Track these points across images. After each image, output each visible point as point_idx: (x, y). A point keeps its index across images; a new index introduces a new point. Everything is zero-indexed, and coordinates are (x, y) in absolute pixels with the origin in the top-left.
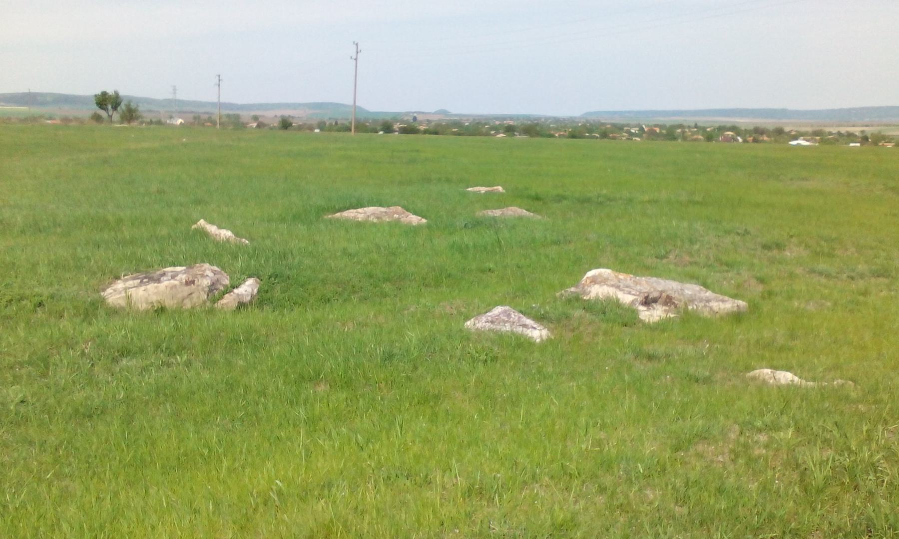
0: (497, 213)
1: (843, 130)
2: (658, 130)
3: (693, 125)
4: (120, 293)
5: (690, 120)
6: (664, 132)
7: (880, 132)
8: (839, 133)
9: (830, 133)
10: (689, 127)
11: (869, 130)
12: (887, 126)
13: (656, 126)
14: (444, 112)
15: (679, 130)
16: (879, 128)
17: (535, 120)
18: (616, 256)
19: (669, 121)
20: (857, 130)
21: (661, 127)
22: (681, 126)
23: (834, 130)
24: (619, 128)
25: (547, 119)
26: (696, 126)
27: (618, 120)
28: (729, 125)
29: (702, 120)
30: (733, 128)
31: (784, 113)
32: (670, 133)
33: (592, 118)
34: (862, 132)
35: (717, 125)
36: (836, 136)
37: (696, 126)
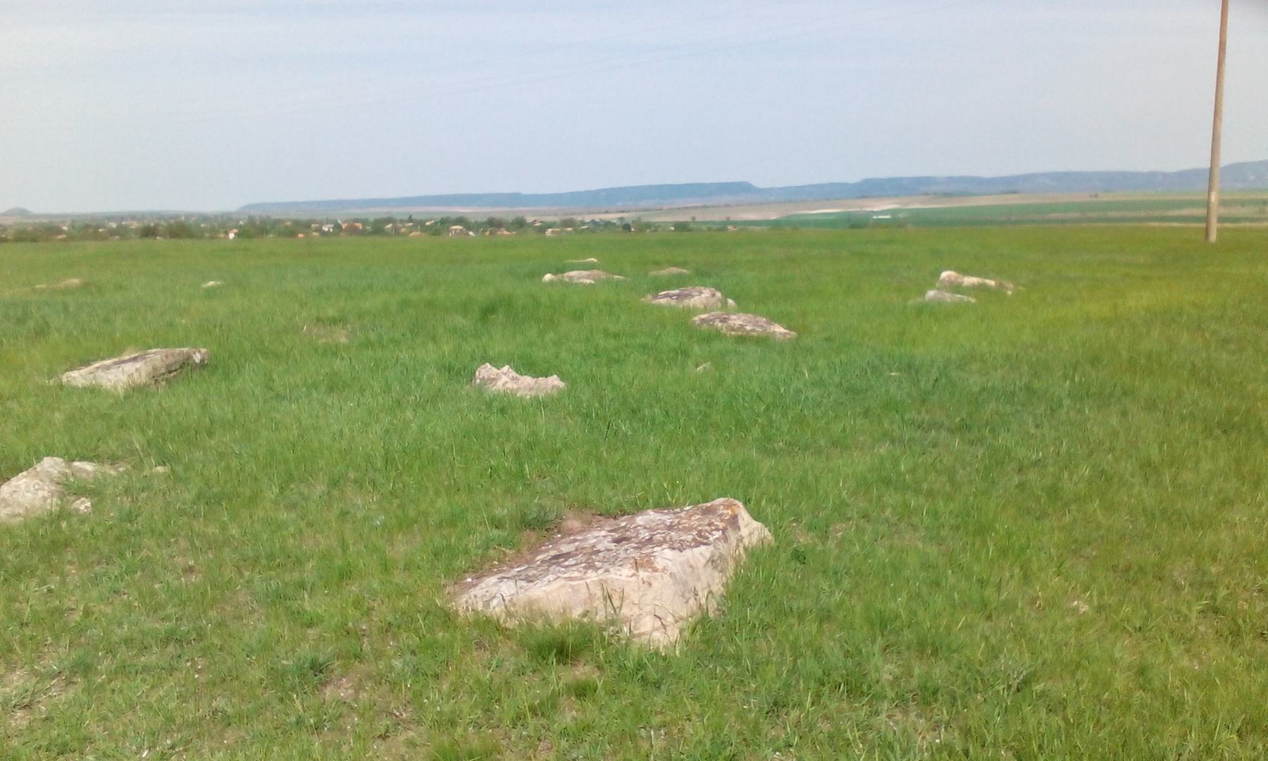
0: (1139, 300)
1: (597, 218)
2: (360, 226)
3: (406, 217)
4: (1042, 695)
5: (399, 212)
6: (368, 228)
7: (639, 219)
8: (593, 222)
9: (583, 223)
10: (402, 221)
11: (629, 217)
12: (646, 210)
13: (357, 221)
14: (22, 212)
15: (390, 226)
16: (620, 215)
17: (171, 218)
18: (12, 536)
19: (374, 213)
20: (613, 217)
21: (364, 222)
22: (389, 220)
23: (588, 219)
24: (306, 226)
25: (189, 216)
26: (410, 220)
27: (304, 217)
28: (454, 217)
29: (418, 211)
30: (460, 221)
31: (515, 198)
32: (377, 228)
33: (256, 213)
34: (621, 219)
35: (439, 218)
36: (592, 226)
37: (410, 220)
